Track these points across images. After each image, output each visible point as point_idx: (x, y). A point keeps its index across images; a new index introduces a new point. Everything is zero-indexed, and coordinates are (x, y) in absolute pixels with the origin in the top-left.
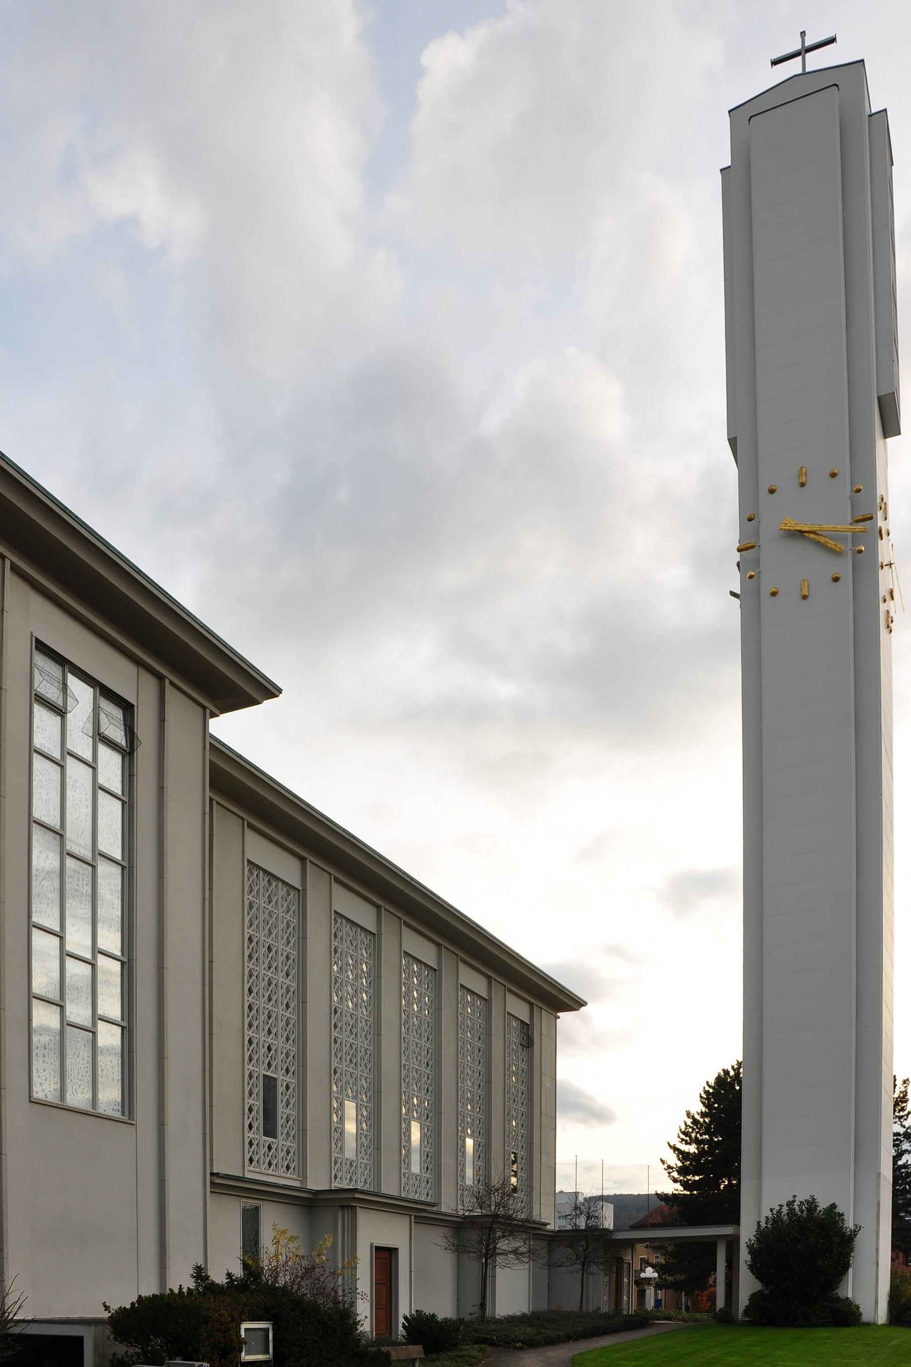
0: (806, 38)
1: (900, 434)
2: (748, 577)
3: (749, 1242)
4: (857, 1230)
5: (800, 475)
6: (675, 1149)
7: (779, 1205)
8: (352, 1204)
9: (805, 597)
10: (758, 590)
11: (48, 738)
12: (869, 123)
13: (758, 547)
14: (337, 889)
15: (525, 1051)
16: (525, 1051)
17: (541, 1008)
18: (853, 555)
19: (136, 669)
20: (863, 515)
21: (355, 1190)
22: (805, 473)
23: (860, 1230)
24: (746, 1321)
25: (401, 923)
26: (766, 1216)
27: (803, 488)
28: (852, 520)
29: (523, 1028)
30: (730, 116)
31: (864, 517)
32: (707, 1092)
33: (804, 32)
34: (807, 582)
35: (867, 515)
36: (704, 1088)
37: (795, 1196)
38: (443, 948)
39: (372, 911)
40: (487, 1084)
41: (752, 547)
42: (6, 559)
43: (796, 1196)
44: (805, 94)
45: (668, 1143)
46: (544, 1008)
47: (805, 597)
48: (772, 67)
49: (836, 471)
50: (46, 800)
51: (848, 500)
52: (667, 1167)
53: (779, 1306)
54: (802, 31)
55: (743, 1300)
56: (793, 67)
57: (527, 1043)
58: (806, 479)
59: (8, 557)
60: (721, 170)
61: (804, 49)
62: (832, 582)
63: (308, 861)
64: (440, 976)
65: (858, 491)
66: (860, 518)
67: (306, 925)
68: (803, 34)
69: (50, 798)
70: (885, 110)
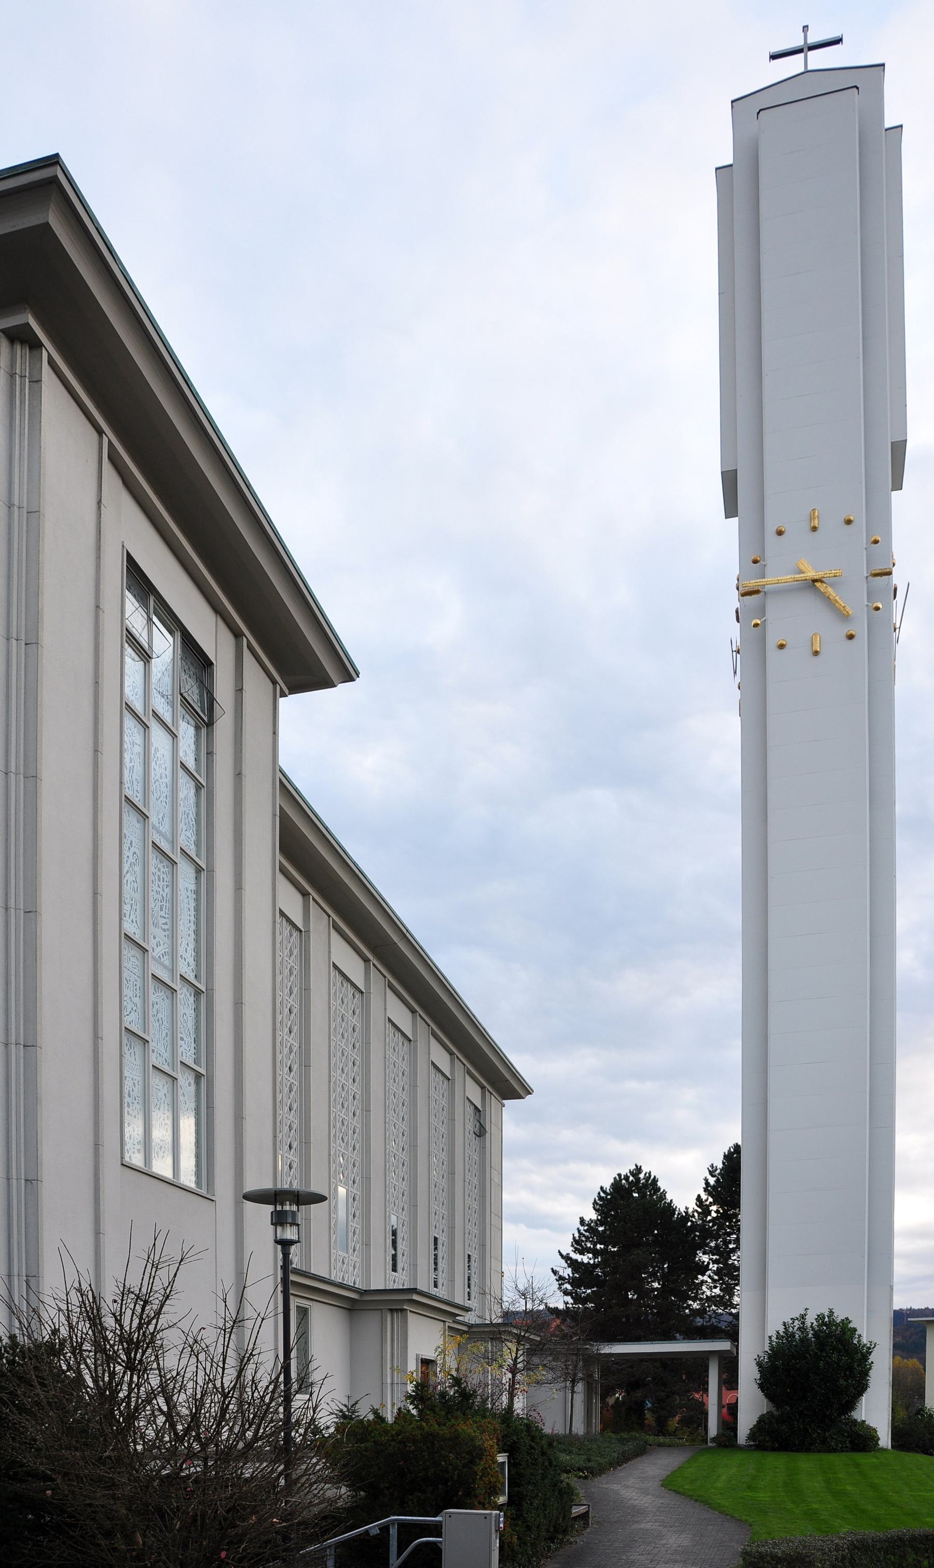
0: (808, 33)
2: (753, 624)
4: (872, 1346)
5: (812, 518)
6: (567, 1258)
7: (792, 1319)
8: (405, 1307)
9: (816, 653)
10: (762, 641)
11: (131, 688)
17: (491, 1094)
18: (868, 611)
19: (215, 619)
20: (881, 569)
21: (414, 1291)
22: (818, 516)
23: (875, 1346)
24: (751, 1446)
27: (816, 533)
28: (867, 573)
30: (732, 107)
32: (600, 1198)
33: (807, 26)
34: (818, 637)
35: (886, 569)
36: (599, 1193)
39: (360, 963)
41: (757, 592)
42: (104, 435)
44: (842, 88)
45: (559, 1252)
47: (816, 653)
49: (852, 518)
50: (130, 767)
52: (559, 1278)
53: (795, 1429)
54: (806, 24)
55: (746, 1422)
56: (794, 65)
57: (478, 1131)
58: (818, 524)
59: (107, 433)
60: (716, 169)
62: (846, 638)
63: (311, 897)
64: (416, 1048)
65: (876, 542)
66: (878, 572)
67: (310, 973)
68: (806, 29)
69: (133, 766)
70: (901, 126)
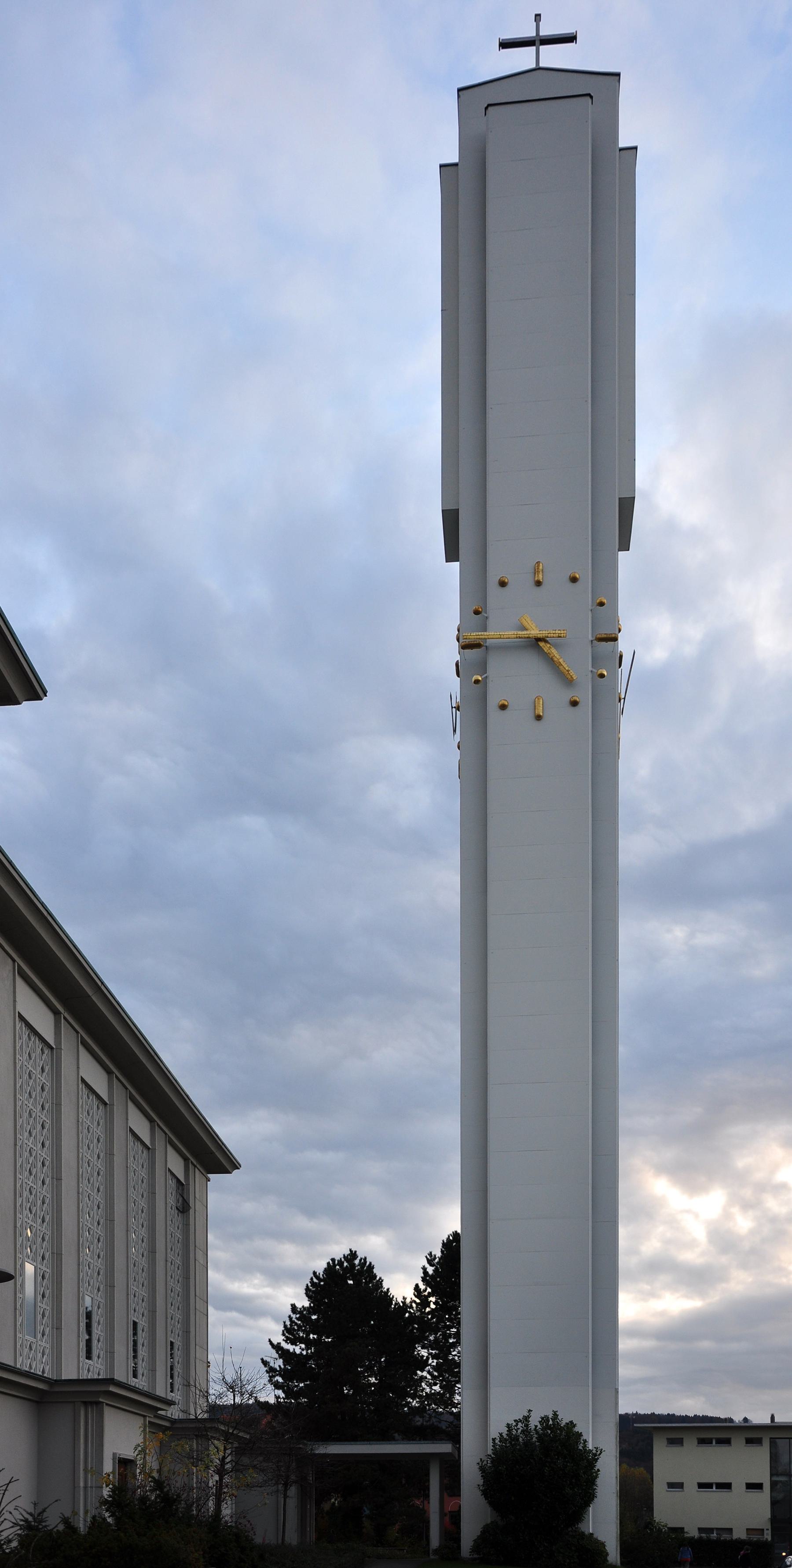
0: (541, 23)
1: (628, 550)
2: (473, 681)
3: (480, 1463)
5: (536, 571)
12: (620, 158)
13: (485, 647)
14: (22, 987)
15: (180, 1217)
16: (180, 1217)
25: (78, 1041)
26: (499, 1433)
28: (592, 637)
29: (178, 1189)
30: (459, 96)
31: (608, 636)
34: (541, 700)
35: (612, 634)
37: (530, 1411)
38: (115, 1079)
40: (151, 1254)
43: (532, 1411)
45: (270, 1341)
46: (198, 1166)
47: (539, 718)
48: (499, 50)
51: (590, 613)
56: (523, 59)
58: (543, 578)
60: (441, 166)
61: (539, 38)
65: (601, 604)
68: (538, 17)
